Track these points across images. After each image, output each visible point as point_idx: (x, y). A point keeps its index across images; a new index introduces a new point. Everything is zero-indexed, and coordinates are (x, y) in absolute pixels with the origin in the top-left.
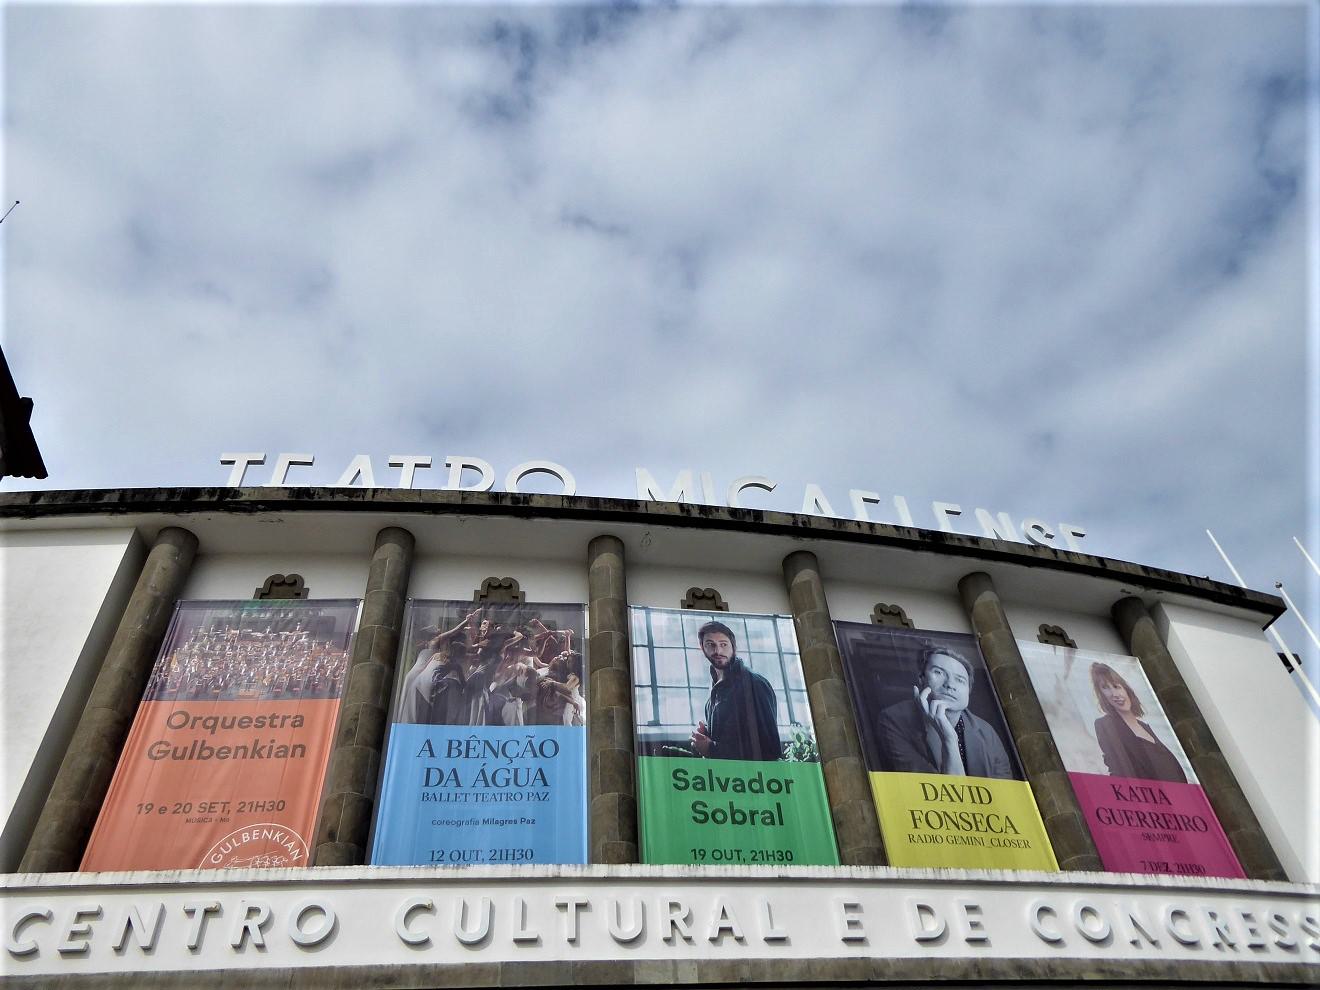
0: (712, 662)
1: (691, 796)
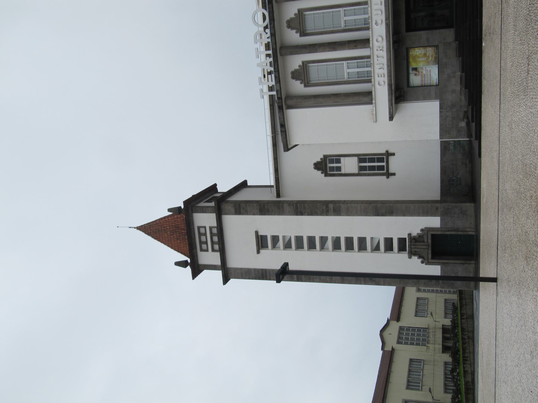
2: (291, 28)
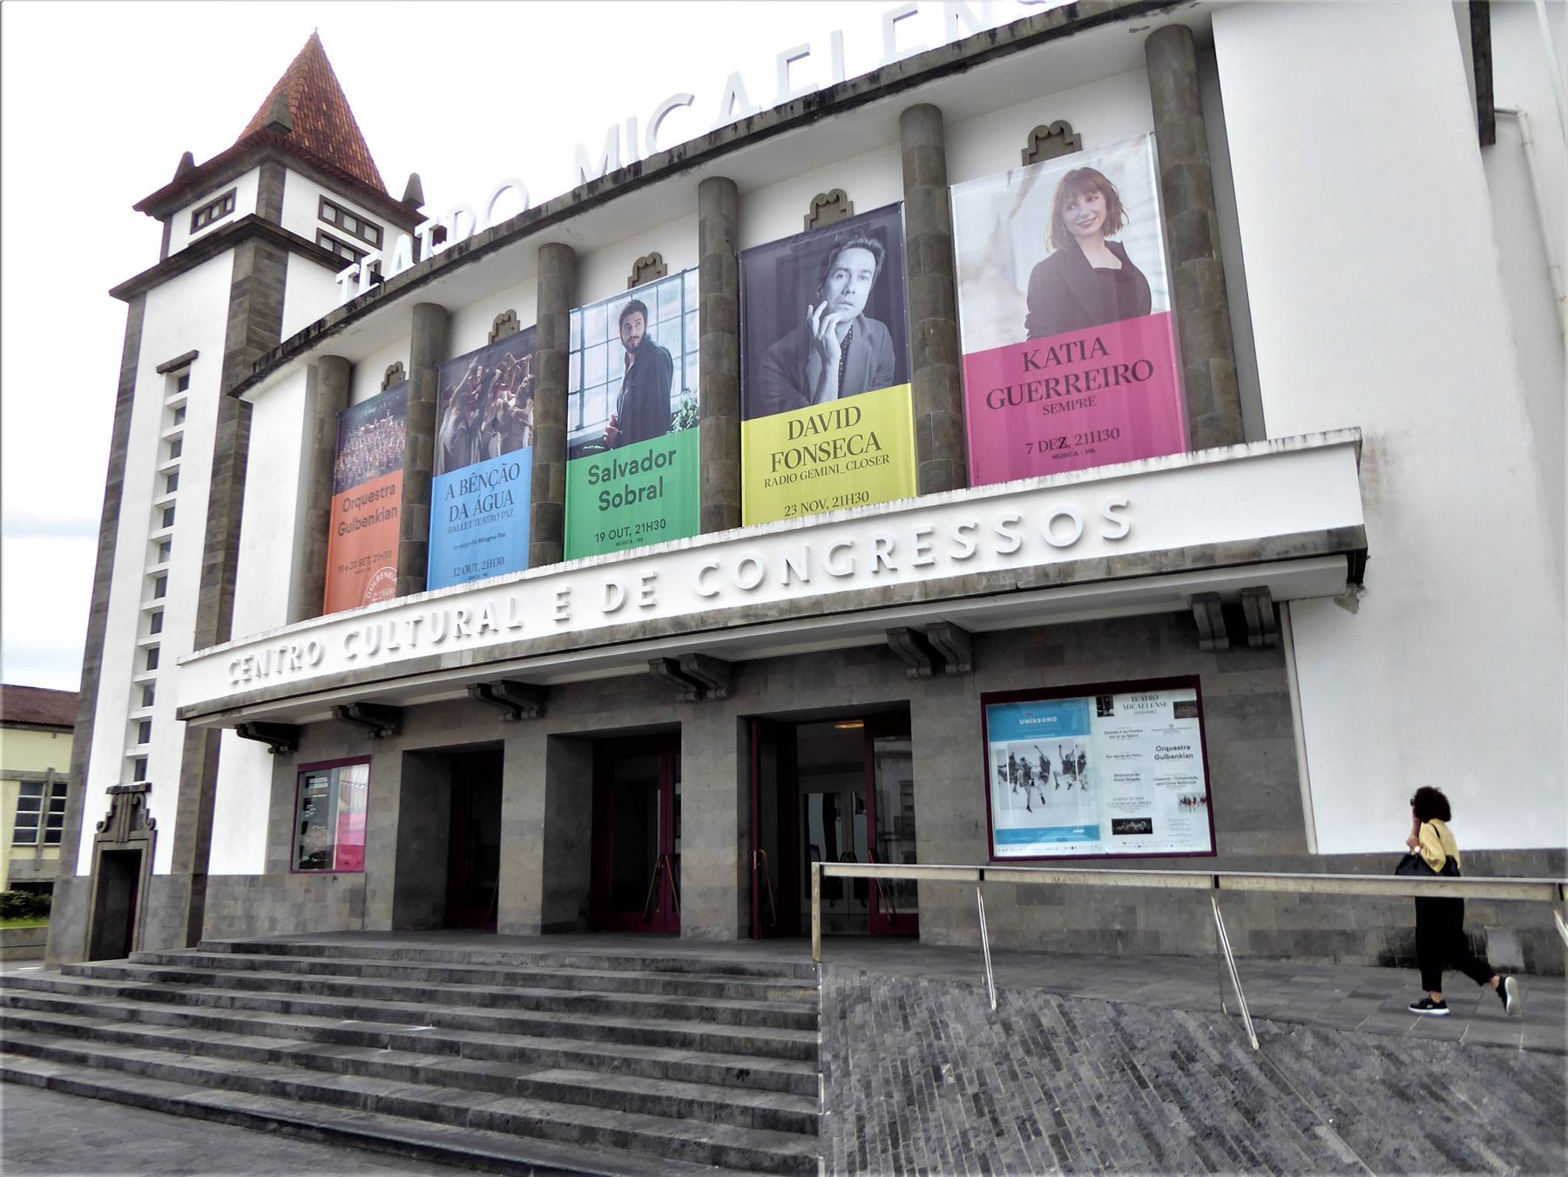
0: (627, 347)
1: (600, 487)
2: (1034, 150)
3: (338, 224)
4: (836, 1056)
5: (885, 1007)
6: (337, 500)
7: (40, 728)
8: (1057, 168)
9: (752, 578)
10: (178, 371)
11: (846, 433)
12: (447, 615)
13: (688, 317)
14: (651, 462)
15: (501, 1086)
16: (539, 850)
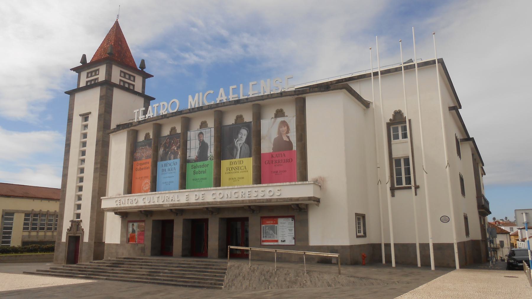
1: (193, 170)
3: (124, 77)
4: (228, 273)
5: (236, 267)
6: (135, 163)
7: (20, 197)
8: (280, 120)
9: (221, 196)
10: (85, 117)
11: (241, 165)
12: (164, 196)
13: (212, 137)
14: (204, 166)
15: (181, 277)
16: (181, 241)
